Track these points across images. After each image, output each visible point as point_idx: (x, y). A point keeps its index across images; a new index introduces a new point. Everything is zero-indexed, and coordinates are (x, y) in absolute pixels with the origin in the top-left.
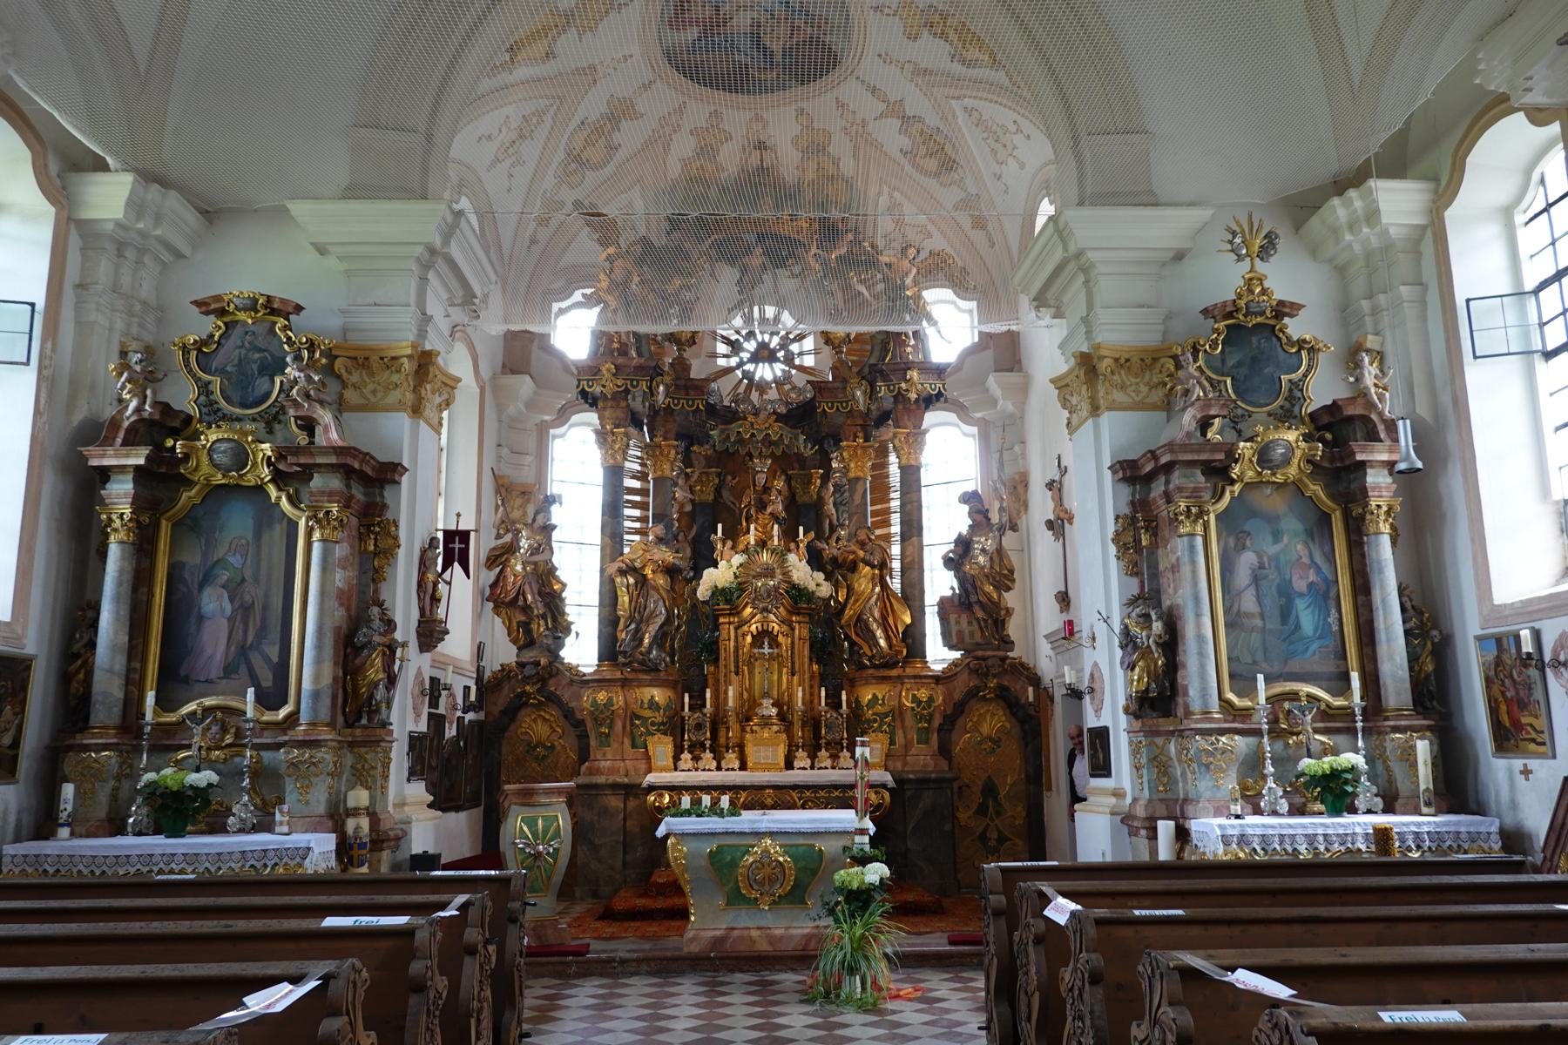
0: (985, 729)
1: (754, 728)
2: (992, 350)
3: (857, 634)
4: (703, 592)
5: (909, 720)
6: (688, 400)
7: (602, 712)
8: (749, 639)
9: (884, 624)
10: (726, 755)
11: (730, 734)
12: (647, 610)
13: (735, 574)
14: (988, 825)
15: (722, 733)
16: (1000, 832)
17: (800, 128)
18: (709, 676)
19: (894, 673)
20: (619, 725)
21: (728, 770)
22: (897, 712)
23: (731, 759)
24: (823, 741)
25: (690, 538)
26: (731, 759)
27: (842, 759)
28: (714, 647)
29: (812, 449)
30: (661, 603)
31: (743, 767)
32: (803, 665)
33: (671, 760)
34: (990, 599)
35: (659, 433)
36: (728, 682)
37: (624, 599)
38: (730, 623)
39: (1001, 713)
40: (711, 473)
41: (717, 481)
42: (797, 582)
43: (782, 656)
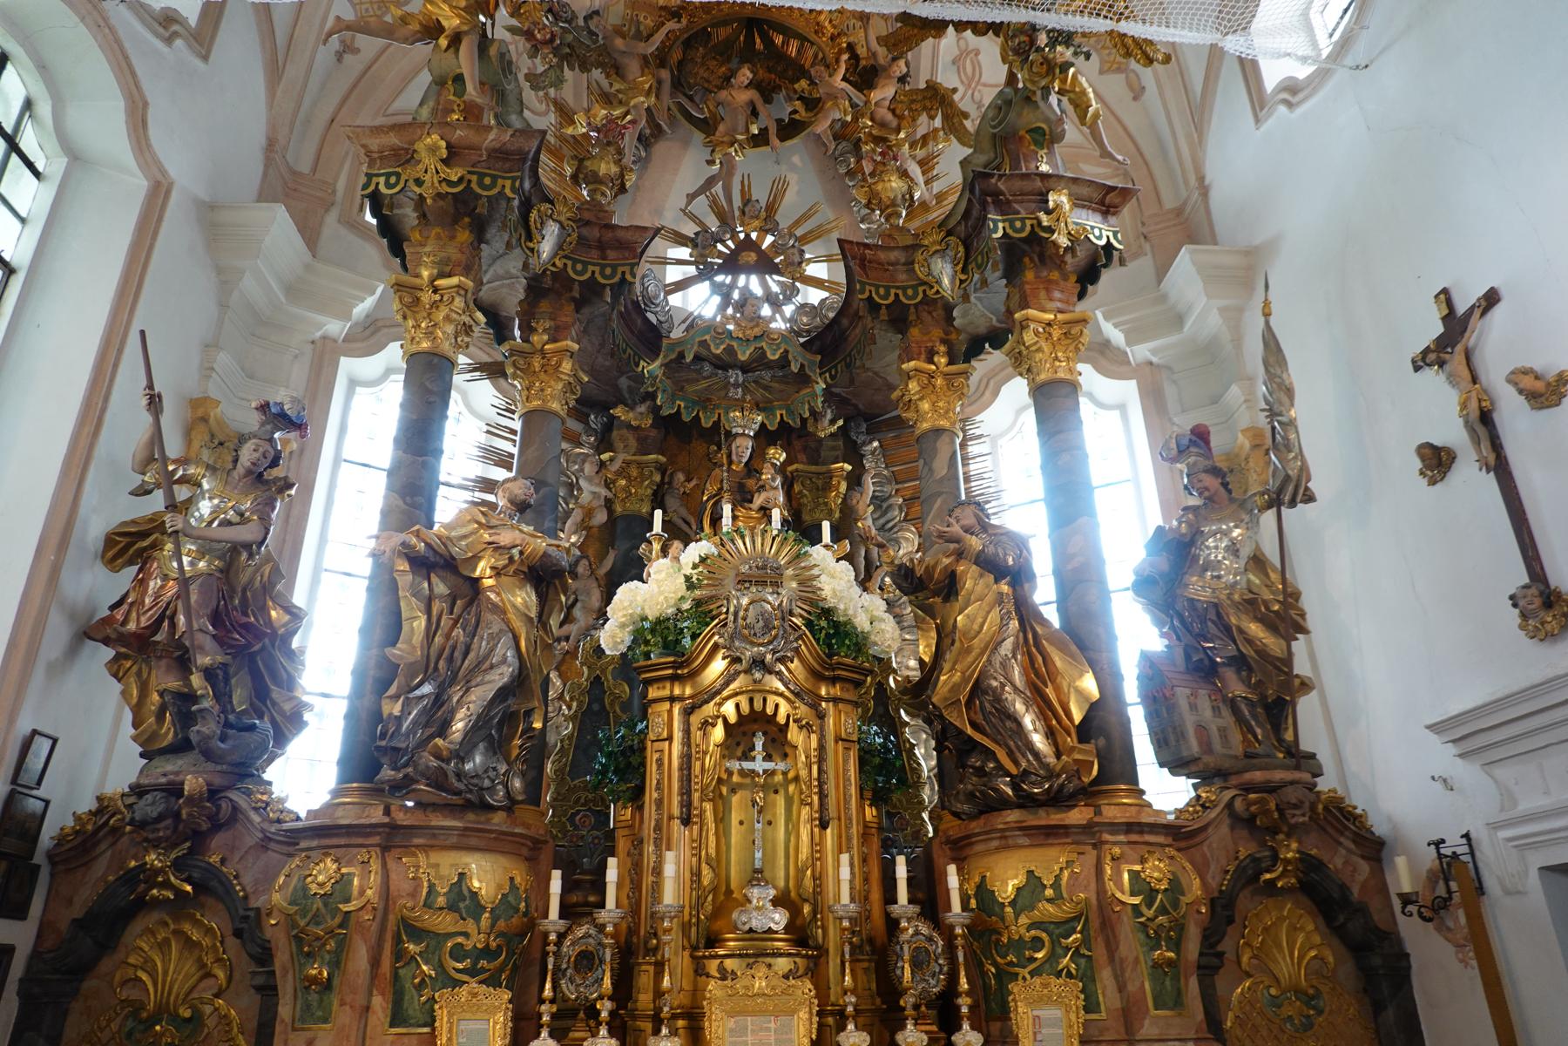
2: (1149, 256)
3: (974, 725)
4: (613, 637)
5: (1130, 942)
6: (603, 267)
7: (316, 919)
8: (718, 733)
11: (666, 982)
12: (472, 656)
13: (688, 578)
15: (645, 979)
18: (620, 833)
19: (1077, 816)
20: (360, 958)
22: (1095, 923)
24: (908, 1001)
25: (602, 571)
28: (634, 760)
29: (833, 422)
30: (506, 640)
34: (1262, 653)
35: (543, 324)
36: (663, 842)
38: (672, 699)
39: (1311, 927)
40: (647, 463)
41: (657, 478)
42: (831, 602)
43: (797, 779)
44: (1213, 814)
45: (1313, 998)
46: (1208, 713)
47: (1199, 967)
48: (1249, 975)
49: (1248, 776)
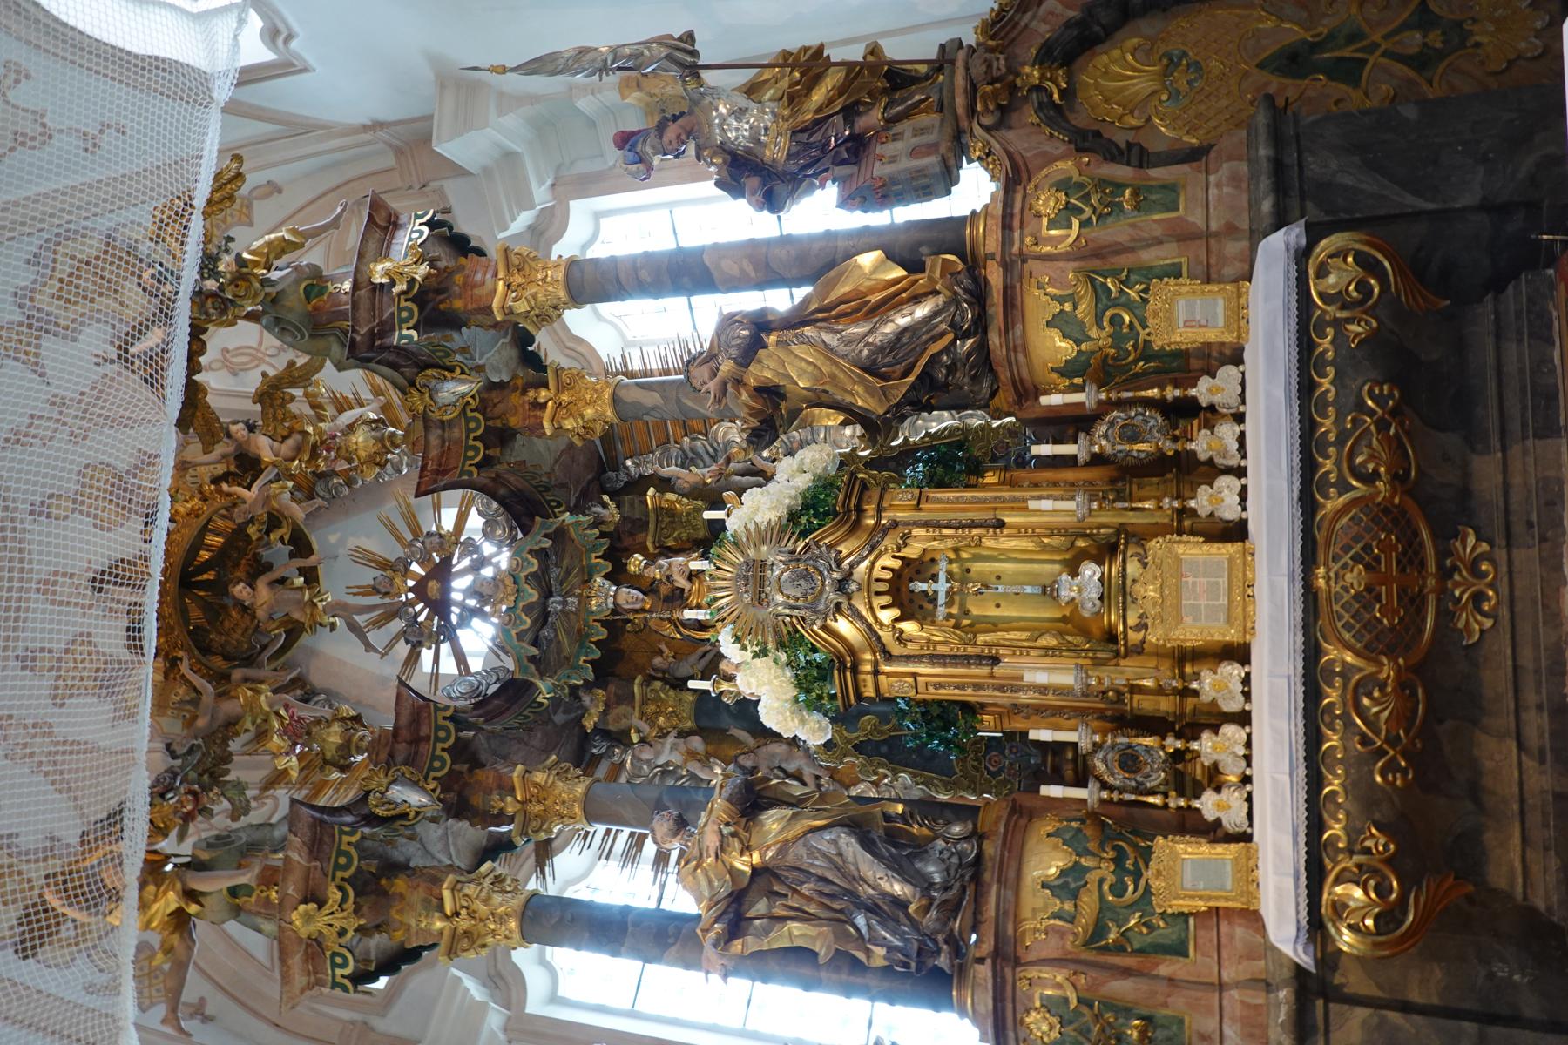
0: (1142, 84)
1: (1132, 621)
2: (444, 183)
3: (905, 374)
4: (814, 731)
5: (1115, 231)
6: (438, 739)
8: (910, 627)
9: (891, 303)
10: (1205, 698)
11: (1148, 683)
12: (829, 875)
13: (756, 655)
14: (1384, 54)
15: (1146, 704)
16: (1405, 26)
17: (77, 515)
20: (1121, 988)
21: (1247, 695)
22: (1096, 264)
23: (1221, 683)
24: (1169, 448)
26: (1221, 683)
27: (1217, 399)
28: (936, 711)
29: (605, 506)
30: (814, 841)
31: (1239, 653)
32: (979, 501)
33: (1220, 849)
36: (1014, 684)
37: (796, 932)
38: (876, 672)
39: (1105, 58)
40: (643, 695)
41: (658, 684)
44: (997, 146)
45: (1171, 60)
46: (899, 145)
47: (1141, 166)
48: (1149, 119)
49: (961, 111)
